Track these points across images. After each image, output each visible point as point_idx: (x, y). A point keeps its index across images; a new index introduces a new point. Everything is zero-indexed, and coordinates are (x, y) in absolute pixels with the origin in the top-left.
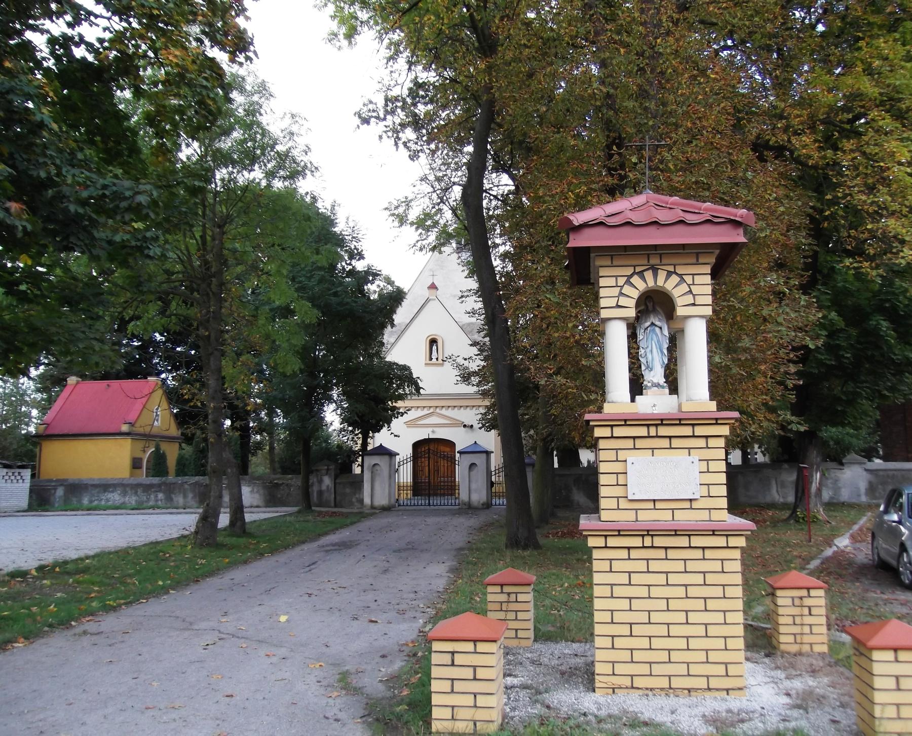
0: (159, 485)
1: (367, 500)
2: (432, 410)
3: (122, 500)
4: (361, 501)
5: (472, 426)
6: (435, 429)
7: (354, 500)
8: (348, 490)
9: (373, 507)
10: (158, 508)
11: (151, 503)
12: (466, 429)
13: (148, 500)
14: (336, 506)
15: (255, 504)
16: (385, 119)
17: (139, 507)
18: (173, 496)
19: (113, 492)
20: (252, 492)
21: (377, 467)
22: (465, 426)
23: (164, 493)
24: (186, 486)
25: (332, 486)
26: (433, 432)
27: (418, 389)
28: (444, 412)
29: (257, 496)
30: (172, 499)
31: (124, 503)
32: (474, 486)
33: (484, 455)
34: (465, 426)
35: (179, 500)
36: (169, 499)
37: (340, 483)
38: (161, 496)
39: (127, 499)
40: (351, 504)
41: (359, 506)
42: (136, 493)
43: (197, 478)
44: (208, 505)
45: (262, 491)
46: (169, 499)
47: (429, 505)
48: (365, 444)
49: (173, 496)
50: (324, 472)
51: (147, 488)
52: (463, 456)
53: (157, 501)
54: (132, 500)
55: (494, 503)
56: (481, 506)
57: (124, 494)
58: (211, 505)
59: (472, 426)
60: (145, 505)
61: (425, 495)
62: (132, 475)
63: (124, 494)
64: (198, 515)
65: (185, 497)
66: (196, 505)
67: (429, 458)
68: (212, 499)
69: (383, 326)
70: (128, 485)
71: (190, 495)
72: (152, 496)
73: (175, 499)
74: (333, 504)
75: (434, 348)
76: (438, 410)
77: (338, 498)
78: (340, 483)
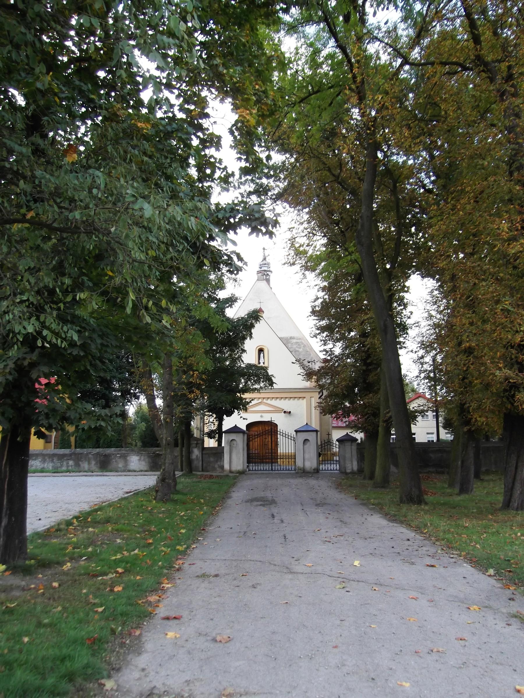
0: (71, 455)
1: (227, 466)
2: (260, 400)
3: (42, 466)
4: (222, 467)
5: (290, 412)
6: (263, 414)
7: (216, 466)
8: (212, 459)
9: (231, 472)
10: (73, 472)
11: (64, 468)
12: (286, 414)
13: (62, 466)
14: (203, 471)
15: (142, 468)
16: (239, 188)
17: (56, 471)
18: (80, 463)
19: (35, 460)
20: (139, 460)
21: (234, 442)
22: (285, 412)
23: (74, 460)
24: (90, 456)
25: (200, 456)
26: (261, 416)
27: (271, 383)
28: (269, 401)
29: (143, 463)
30: (79, 466)
31: (43, 468)
32: (307, 456)
33: (315, 433)
34: (285, 412)
35: (85, 465)
36: (77, 465)
37: (206, 454)
38: (71, 463)
39: (46, 465)
40: (214, 469)
41: (220, 470)
42: (52, 461)
43: (98, 450)
44: (164, 470)
45: (147, 460)
46: (77, 465)
47: (272, 470)
48: (220, 425)
49: (80, 463)
50: (194, 445)
51: (61, 457)
52: (298, 434)
53: (68, 466)
54: (49, 466)
55: (321, 468)
56: (313, 471)
57: (44, 461)
58: (166, 469)
59: (290, 412)
60: (59, 470)
61: (268, 463)
62: (45, 448)
63: (44, 461)
64: (156, 477)
65: (89, 463)
66: (97, 470)
67: (271, 435)
68: (167, 465)
69: (244, 338)
70: (47, 455)
71: (93, 463)
72: (65, 463)
73: (82, 465)
74: (201, 470)
75: (262, 355)
76: (265, 401)
77: (204, 465)
78: (206, 454)
